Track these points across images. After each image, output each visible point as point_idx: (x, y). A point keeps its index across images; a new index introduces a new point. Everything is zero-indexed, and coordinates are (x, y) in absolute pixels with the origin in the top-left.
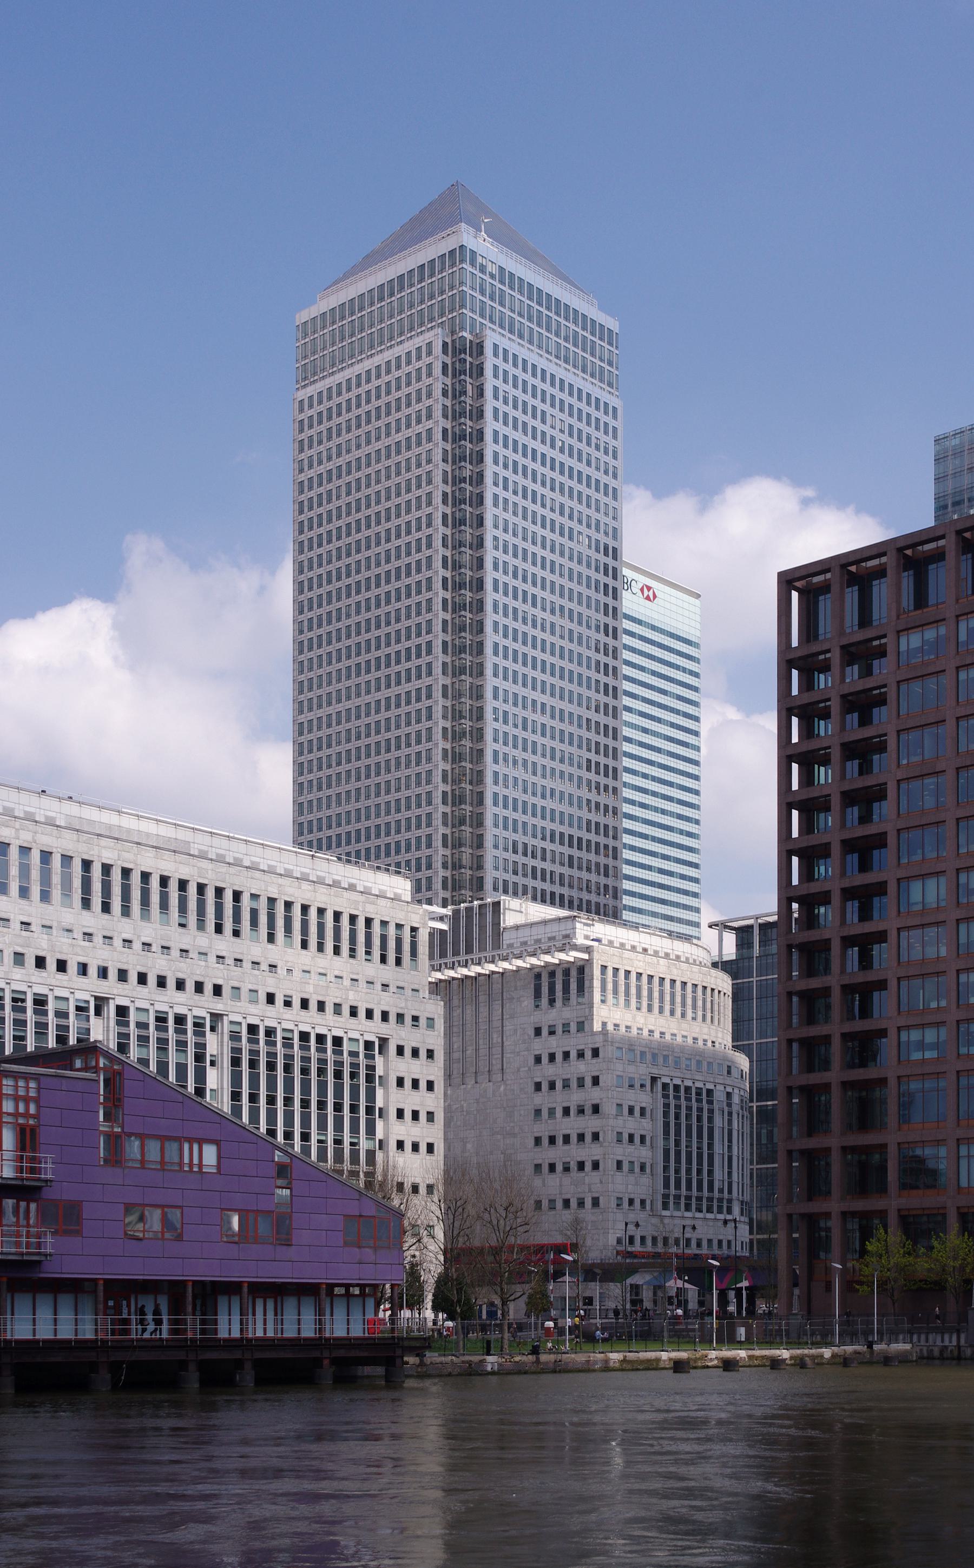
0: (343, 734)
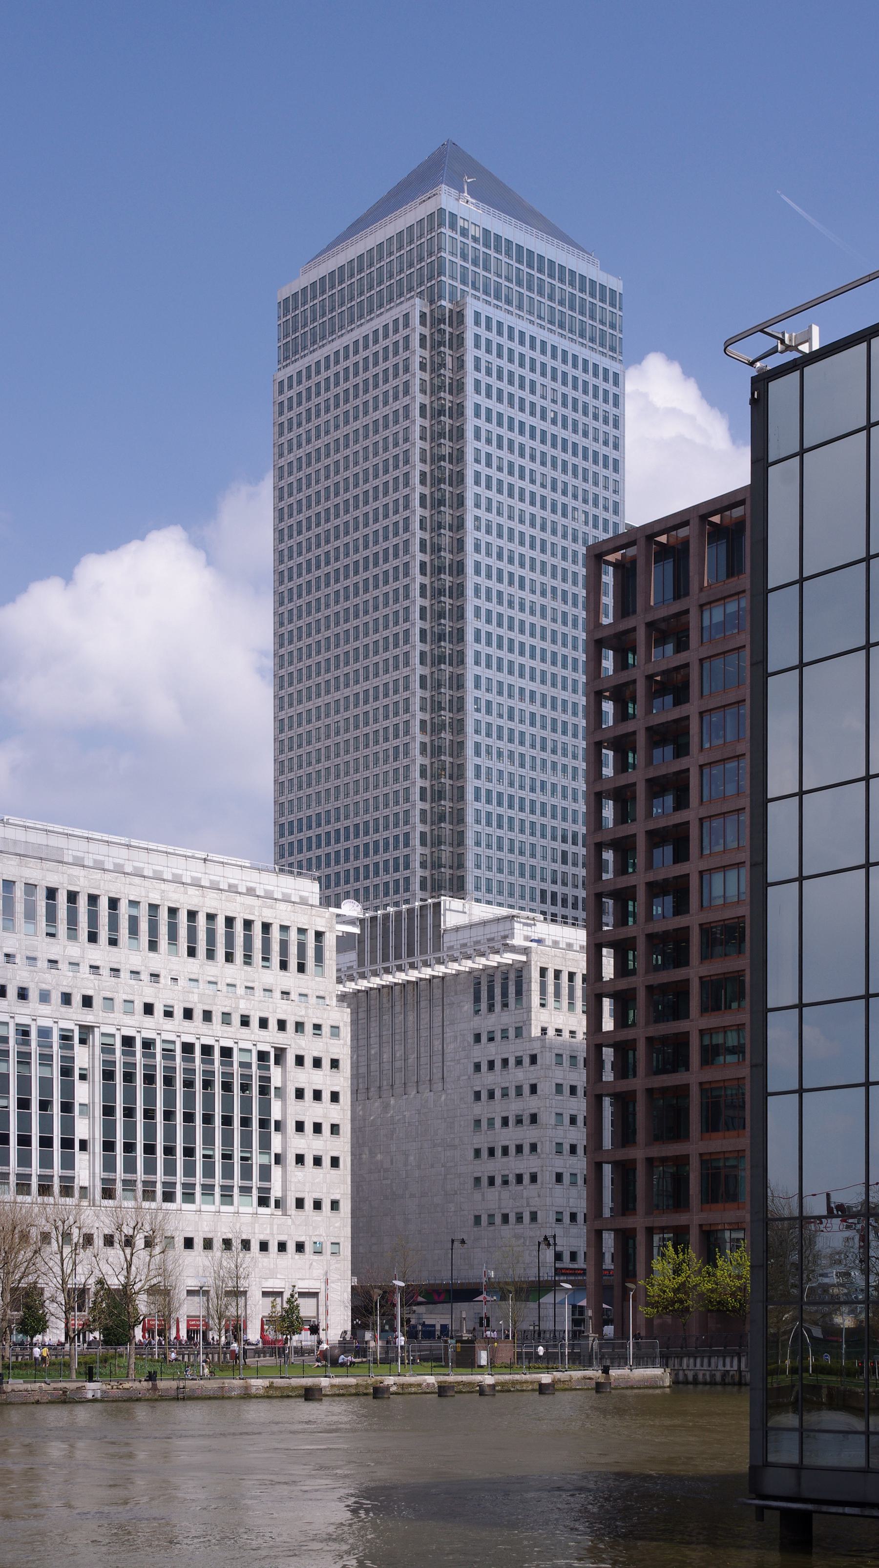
0: (322, 730)
